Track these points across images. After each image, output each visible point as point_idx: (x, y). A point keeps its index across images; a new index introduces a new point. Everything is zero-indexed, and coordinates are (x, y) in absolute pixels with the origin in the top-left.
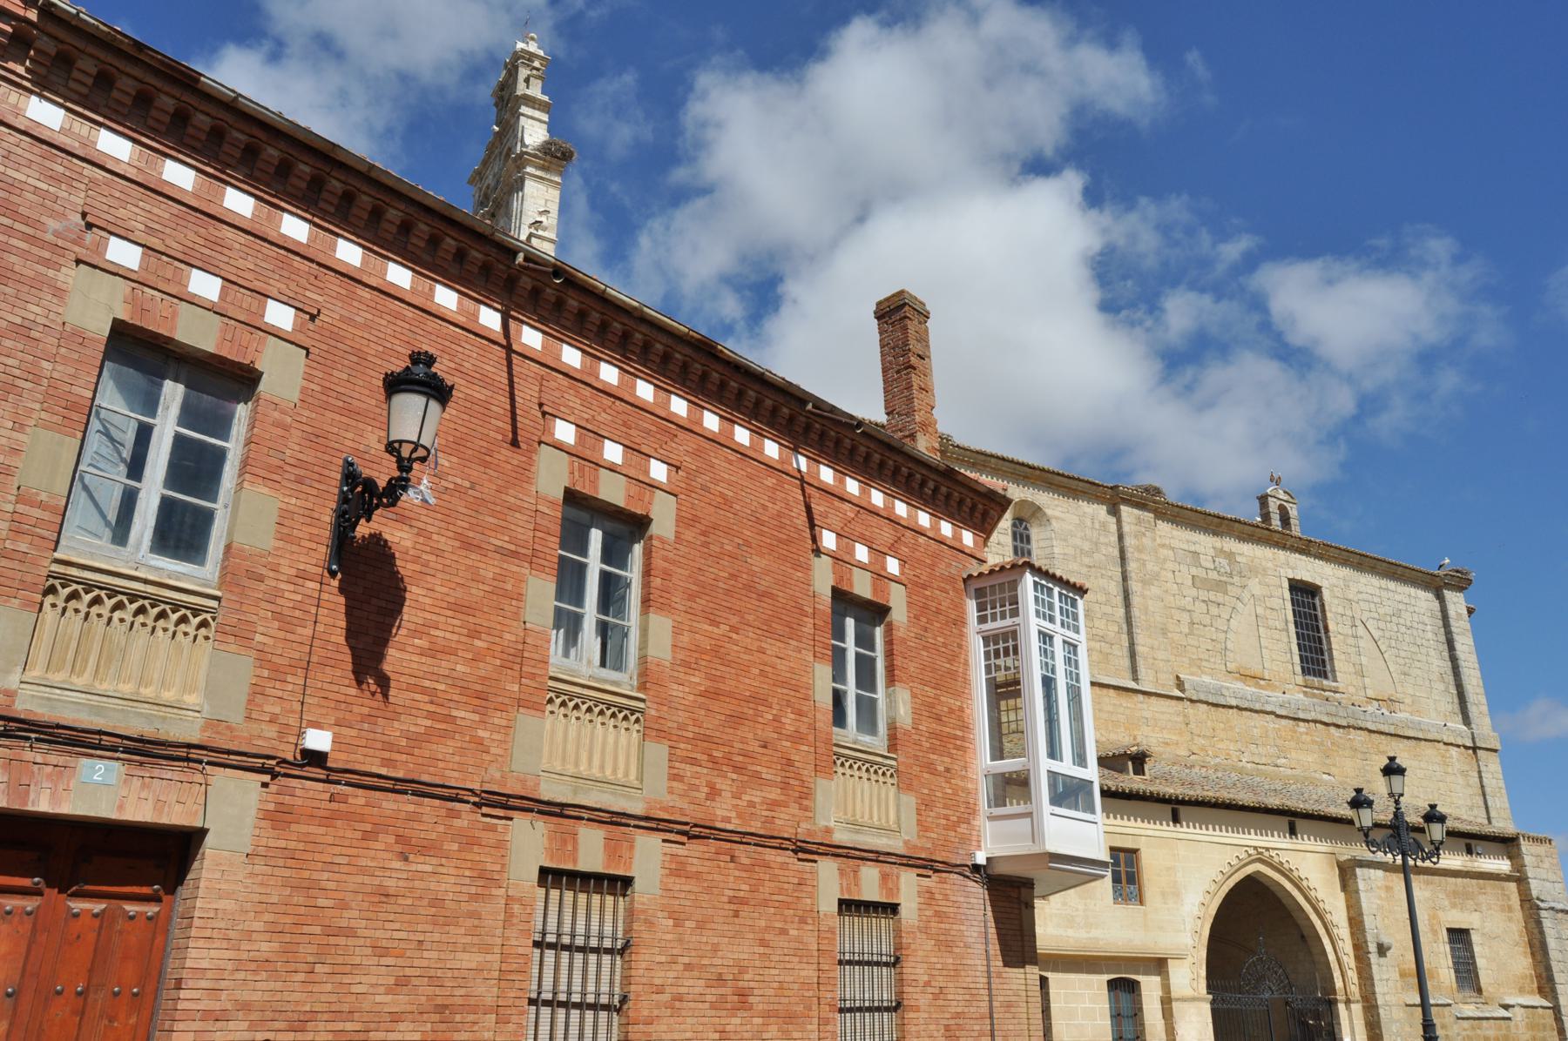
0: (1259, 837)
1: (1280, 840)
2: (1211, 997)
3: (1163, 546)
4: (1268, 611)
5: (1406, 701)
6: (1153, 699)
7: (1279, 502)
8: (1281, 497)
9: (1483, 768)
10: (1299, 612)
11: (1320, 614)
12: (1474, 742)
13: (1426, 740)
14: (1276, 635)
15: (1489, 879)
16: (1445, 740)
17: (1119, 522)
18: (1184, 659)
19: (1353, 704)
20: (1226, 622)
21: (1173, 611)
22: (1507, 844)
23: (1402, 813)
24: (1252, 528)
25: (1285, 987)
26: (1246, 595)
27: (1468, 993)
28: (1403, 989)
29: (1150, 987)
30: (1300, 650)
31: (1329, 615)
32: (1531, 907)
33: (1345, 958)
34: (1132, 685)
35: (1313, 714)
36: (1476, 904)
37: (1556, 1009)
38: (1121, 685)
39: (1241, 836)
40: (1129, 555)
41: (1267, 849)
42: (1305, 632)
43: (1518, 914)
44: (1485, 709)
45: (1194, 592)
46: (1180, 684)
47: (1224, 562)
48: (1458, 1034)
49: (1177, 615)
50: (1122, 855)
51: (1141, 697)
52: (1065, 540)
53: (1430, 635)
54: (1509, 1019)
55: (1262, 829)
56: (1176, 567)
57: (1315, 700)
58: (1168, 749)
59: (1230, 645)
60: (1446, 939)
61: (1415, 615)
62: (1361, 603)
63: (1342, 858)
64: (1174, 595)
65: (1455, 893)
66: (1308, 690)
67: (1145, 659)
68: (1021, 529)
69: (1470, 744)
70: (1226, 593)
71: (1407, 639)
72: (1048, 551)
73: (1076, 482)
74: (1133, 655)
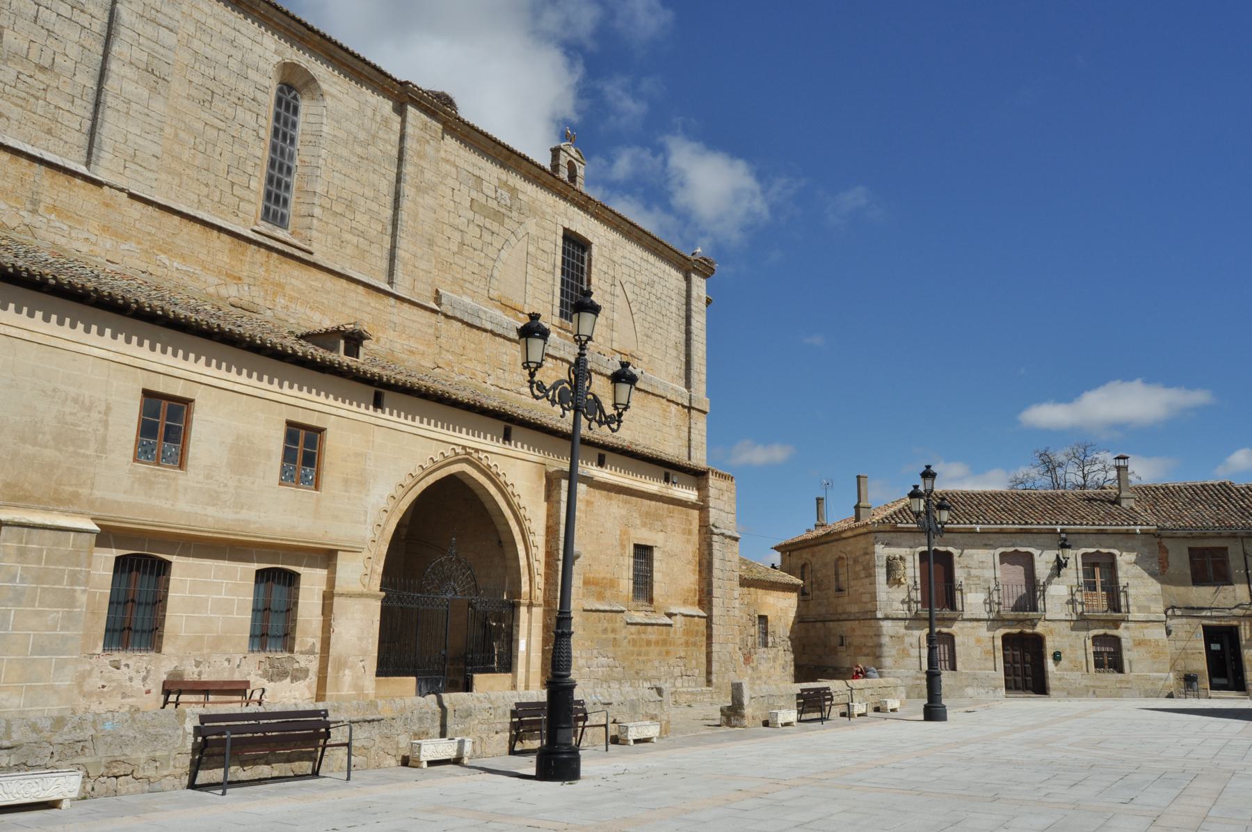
0: (470, 437)
1: (491, 443)
2: (383, 594)
3: (447, 161)
4: (540, 252)
5: (644, 359)
6: (406, 306)
7: (569, 158)
8: (572, 154)
9: (693, 425)
10: (568, 261)
11: (586, 268)
12: (690, 403)
13: (653, 394)
14: (543, 275)
15: (679, 505)
16: (669, 397)
17: (403, 122)
18: (447, 276)
19: (599, 353)
20: (496, 251)
21: (445, 226)
22: (697, 476)
23: (585, 360)
24: (538, 170)
25: (469, 588)
26: (521, 232)
27: (642, 602)
28: (584, 596)
29: (312, 581)
30: (562, 295)
31: (594, 269)
32: (706, 531)
33: (536, 564)
34: (387, 287)
35: (562, 352)
36: (664, 526)
37: (709, 619)
38: (373, 283)
39: (451, 432)
40: (407, 157)
41: (477, 451)
42: (570, 280)
43: (695, 538)
44: (704, 377)
45: (470, 215)
46: (438, 298)
47: (506, 195)
48: (625, 638)
49: (448, 231)
50: (302, 433)
51: (392, 301)
52: (338, 122)
53: (674, 309)
54: (670, 625)
55: (474, 429)
56: (457, 186)
57: (567, 342)
58: (412, 358)
59: (496, 273)
60: (632, 554)
61: (665, 289)
62: (623, 267)
63: (551, 470)
64: (449, 212)
65: (648, 514)
66: (562, 331)
67: (405, 264)
68: (289, 97)
69: (686, 404)
70: (502, 224)
71: (655, 307)
72: (315, 127)
73: (361, 64)
74: (392, 258)
